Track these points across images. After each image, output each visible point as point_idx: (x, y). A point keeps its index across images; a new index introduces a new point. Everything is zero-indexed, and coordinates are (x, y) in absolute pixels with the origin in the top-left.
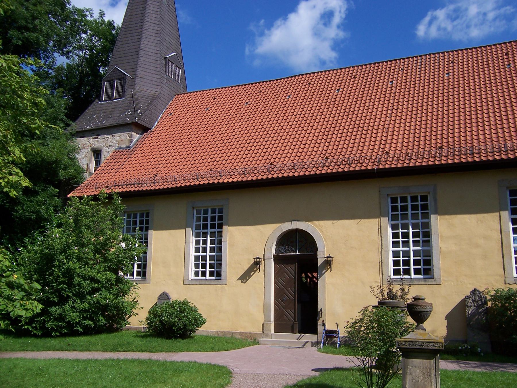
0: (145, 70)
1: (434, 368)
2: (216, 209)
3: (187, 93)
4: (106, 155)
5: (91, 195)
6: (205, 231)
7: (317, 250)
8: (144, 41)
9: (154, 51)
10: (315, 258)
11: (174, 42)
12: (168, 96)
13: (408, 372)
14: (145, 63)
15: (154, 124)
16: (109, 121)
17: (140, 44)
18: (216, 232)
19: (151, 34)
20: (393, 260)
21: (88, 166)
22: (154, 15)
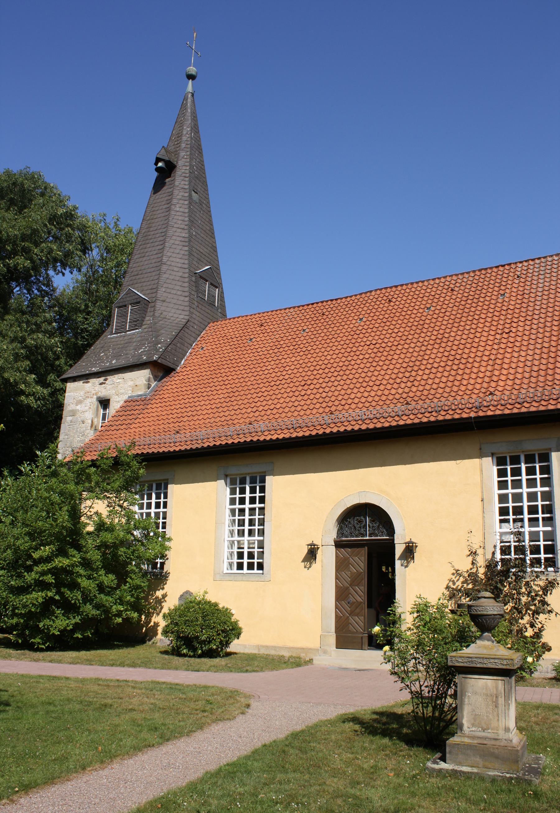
0: (168, 290)
1: (503, 695)
2: (256, 477)
3: (225, 320)
4: (115, 406)
5: (112, 457)
6: (242, 506)
7: (394, 533)
8: (167, 253)
9: (179, 265)
10: (391, 545)
11: (208, 251)
12: (199, 324)
13: (466, 700)
14: (168, 281)
15: (181, 363)
16: (120, 360)
17: (162, 257)
18: (257, 509)
19: (177, 243)
20: (500, 508)
21: (92, 422)
22: (180, 218)
